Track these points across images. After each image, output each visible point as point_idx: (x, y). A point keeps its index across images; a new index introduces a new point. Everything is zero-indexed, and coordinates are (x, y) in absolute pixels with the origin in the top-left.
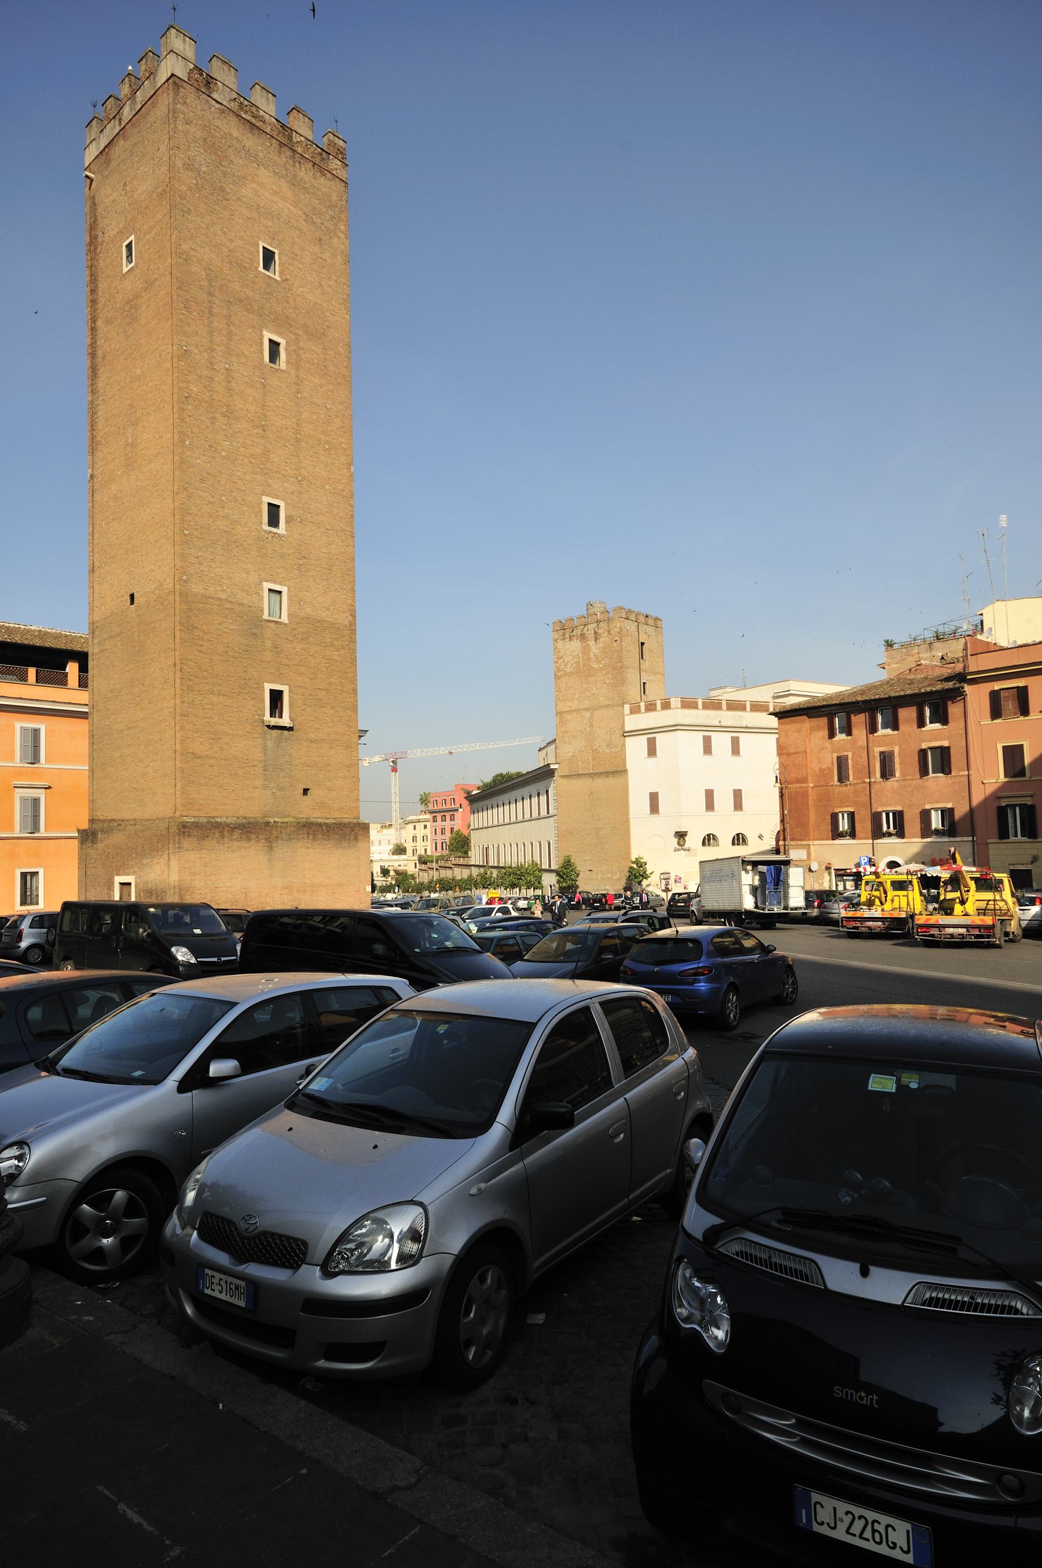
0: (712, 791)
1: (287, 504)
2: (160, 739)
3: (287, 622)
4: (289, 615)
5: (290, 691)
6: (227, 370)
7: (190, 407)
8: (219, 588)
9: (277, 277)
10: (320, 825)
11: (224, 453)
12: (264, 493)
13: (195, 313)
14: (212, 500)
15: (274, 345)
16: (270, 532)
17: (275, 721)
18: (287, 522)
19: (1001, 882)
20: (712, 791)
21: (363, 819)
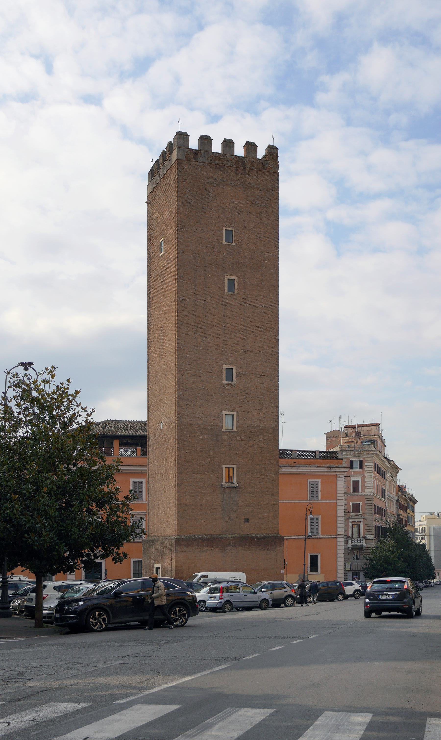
0: (256, 173)
1: (237, 366)
2: (171, 497)
3: (236, 431)
4: (237, 427)
5: (237, 468)
6: (204, 303)
7: (183, 329)
8: (198, 419)
9: (234, 244)
10: (253, 538)
11: (201, 348)
12: (224, 364)
13: (187, 279)
14: (194, 374)
15: (231, 282)
16: (227, 384)
17: (230, 484)
18: (237, 376)
19: (135, 483)
20: (256, 173)
21: (281, 534)
